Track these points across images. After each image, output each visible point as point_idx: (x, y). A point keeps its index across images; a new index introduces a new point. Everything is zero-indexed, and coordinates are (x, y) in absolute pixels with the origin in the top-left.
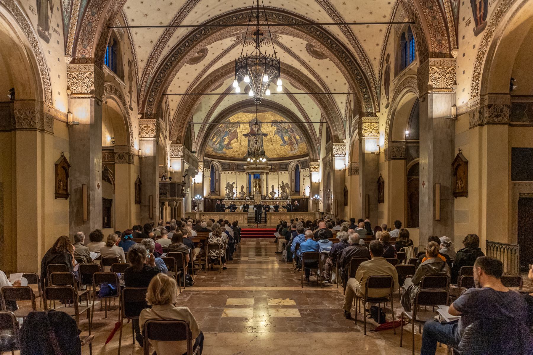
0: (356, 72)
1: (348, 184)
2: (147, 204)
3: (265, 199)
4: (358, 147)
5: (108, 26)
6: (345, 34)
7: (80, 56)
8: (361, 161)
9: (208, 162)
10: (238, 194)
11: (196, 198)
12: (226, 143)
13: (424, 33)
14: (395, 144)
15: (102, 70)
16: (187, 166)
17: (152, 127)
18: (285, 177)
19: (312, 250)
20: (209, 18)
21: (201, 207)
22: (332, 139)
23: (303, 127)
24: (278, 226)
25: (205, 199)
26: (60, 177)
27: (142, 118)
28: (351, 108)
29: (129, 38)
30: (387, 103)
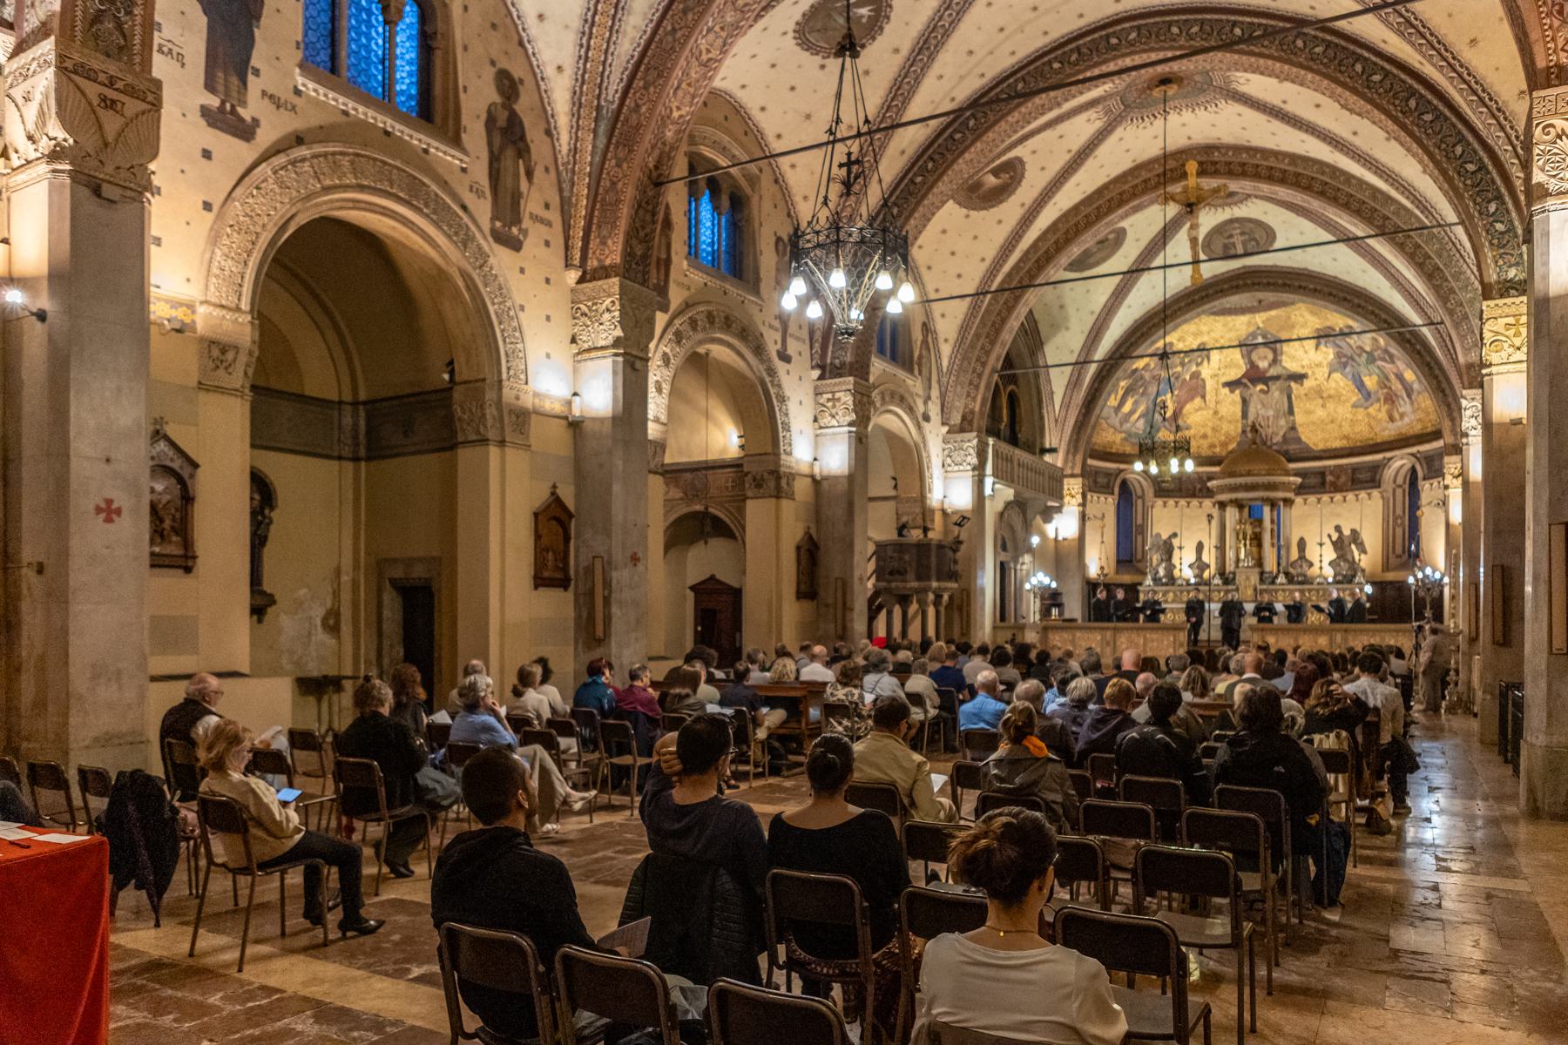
2: (830, 601)
3: (1273, 583)
6: (1401, 34)
7: (596, 263)
19: (982, 725)
20: (984, 81)
26: (545, 541)
27: (821, 378)
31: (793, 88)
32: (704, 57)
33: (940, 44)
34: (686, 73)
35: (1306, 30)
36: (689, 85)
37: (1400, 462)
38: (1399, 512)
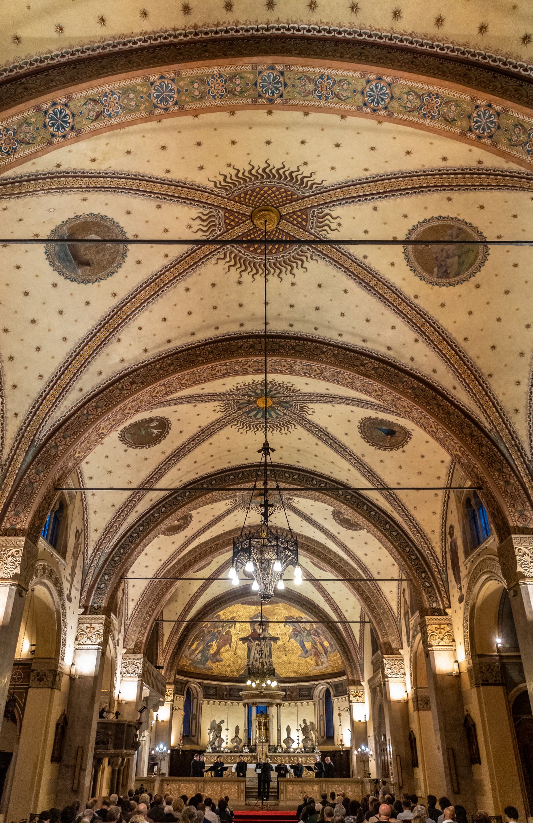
0: (408, 549)
1: (415, 727)
2: (71, 762)
3: (275, 752)
4: (423, 661)
5: (57, 487)
6: (386, 498)
7: (8, 526)
8: (435, 690)
9: (182, 683)
10: (229, 741)
11: (157, 749)
12: (212, 652)
13: (497, 502)
14: (483, 660)
15: (36, 545)
16: (146, 692)
17: (97, 628)
18: (308, 712)
20: (197, 476)
21: (165, 767)
22: (382, 649)
23: (333, 627)
24: (300, 808)
25: (173, 750)
28: (405, 600)
29: (82, 500)
30: (459, 594)
31: (107, 457)
32: (100, 431)
33: (184, 455)
34: (89, 436)
36: (88, 442)
38: (322, 713)
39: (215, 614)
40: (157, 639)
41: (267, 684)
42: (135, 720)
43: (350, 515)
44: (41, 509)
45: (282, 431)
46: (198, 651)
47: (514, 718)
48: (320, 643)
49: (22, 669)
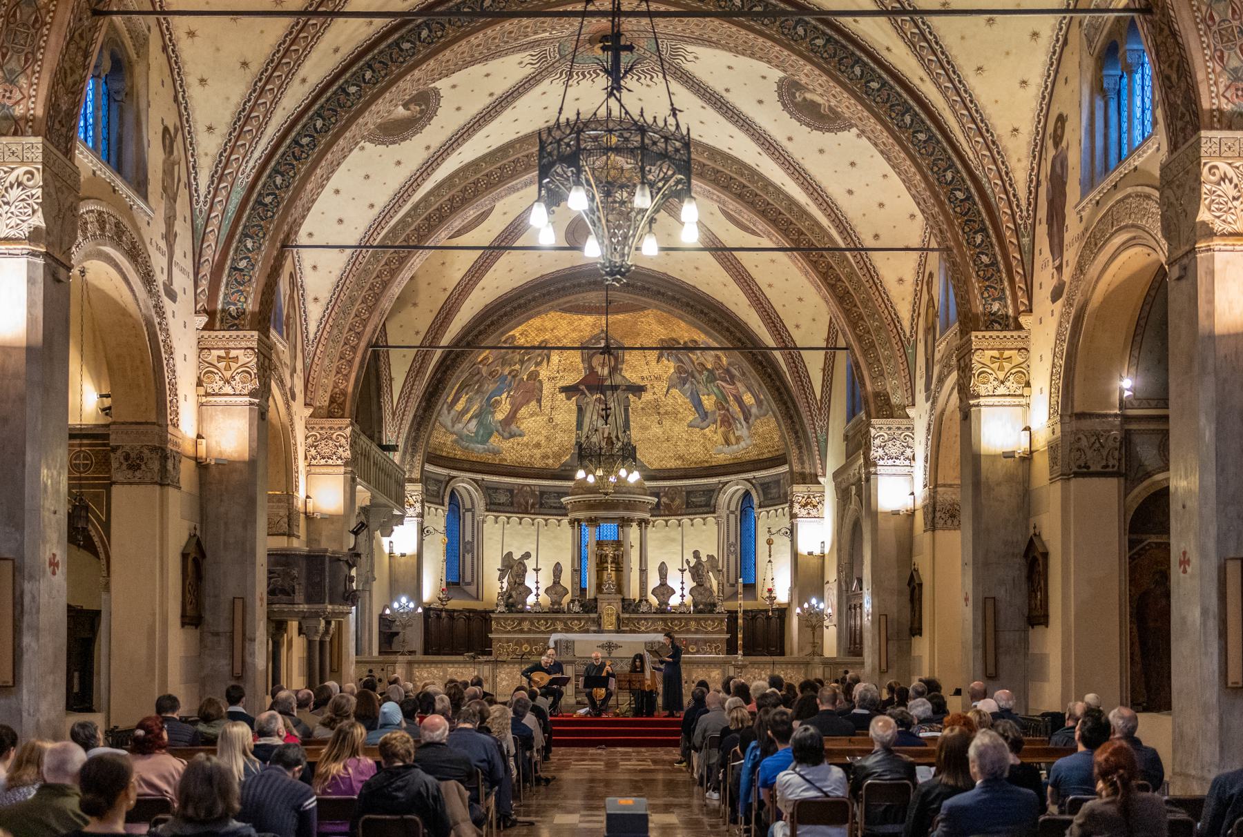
0: (949, 175)
1: (922, 562)
2: (224, 627)
6: (911, 45)
8: (973, 489)
10: (542, 592)
11: (396, 605)
12: (500, 416)
14: (1086, 424)
15: (71, 159)
16: (364, 495)
17: (243, 360)
22: (870, 406)
25: (427, 610)
27: (209, 327)
28: (931, 299)
29: (165, 48)
30: (1055, 282)
35: (807, 18)
37: (734, 487)
38: (732, 539)
39: (503, 334)
40: (379, 389)
41: (619, 478)
42: (345, 550)
43: (820, 91)
44: (67, 66)
45: (642, 80)
46: (469, 415)
47: (1130, 541)
48: (734, 396)
49: (90, 445)
